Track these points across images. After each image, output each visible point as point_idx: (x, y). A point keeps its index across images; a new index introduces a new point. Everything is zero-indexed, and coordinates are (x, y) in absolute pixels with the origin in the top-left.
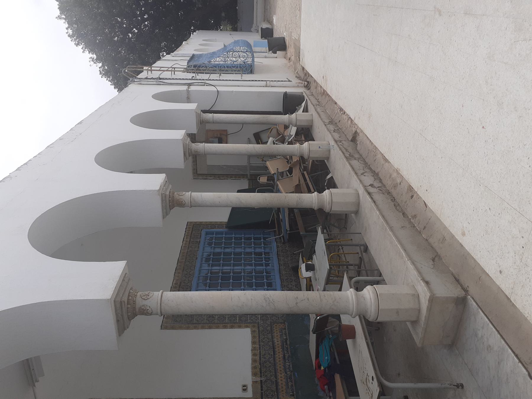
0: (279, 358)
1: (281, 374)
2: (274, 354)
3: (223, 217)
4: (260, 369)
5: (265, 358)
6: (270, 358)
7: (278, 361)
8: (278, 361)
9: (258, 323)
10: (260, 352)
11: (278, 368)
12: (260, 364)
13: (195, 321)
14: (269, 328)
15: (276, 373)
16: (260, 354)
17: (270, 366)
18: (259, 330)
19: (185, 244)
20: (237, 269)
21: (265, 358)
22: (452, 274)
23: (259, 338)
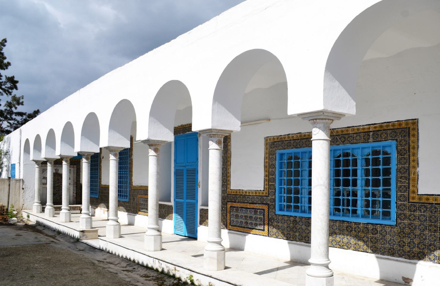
0: (247, 205)
1: (239, 205)
2: (250, 203)
3: (103, 183)
4: (242, 195)
5: (247, 198)
6: (247, 200)
7: (259, 206)
8: (245, 204)
9: (269, 196)
10: (251, 196)
11: (242, 204)
12: (245, 195)
13: (271, 157)
14: (265, 202)
15: (240, 202)
16: (249, 195)
17: (243, 200)
18: (264, 196)
19: (364, 129)
20: (360, 183)
21: (247, 198)
22: (58, 244)
23: (259, 196)
